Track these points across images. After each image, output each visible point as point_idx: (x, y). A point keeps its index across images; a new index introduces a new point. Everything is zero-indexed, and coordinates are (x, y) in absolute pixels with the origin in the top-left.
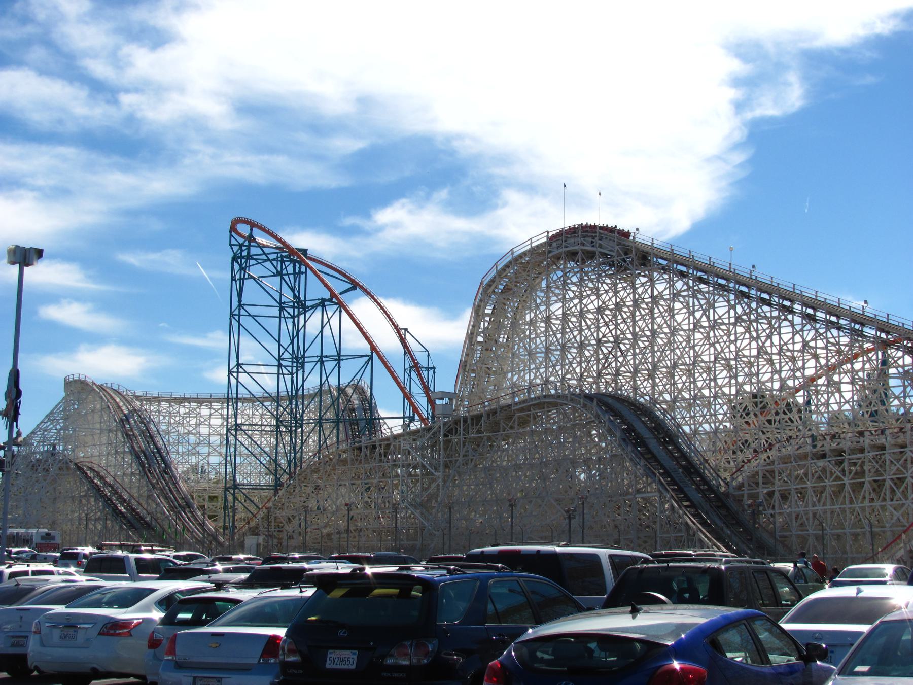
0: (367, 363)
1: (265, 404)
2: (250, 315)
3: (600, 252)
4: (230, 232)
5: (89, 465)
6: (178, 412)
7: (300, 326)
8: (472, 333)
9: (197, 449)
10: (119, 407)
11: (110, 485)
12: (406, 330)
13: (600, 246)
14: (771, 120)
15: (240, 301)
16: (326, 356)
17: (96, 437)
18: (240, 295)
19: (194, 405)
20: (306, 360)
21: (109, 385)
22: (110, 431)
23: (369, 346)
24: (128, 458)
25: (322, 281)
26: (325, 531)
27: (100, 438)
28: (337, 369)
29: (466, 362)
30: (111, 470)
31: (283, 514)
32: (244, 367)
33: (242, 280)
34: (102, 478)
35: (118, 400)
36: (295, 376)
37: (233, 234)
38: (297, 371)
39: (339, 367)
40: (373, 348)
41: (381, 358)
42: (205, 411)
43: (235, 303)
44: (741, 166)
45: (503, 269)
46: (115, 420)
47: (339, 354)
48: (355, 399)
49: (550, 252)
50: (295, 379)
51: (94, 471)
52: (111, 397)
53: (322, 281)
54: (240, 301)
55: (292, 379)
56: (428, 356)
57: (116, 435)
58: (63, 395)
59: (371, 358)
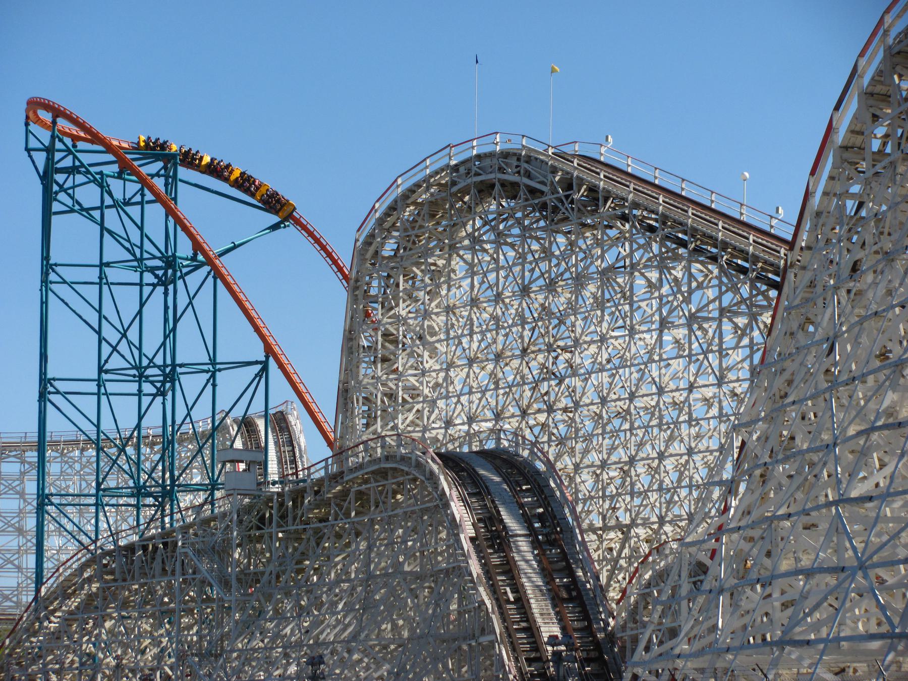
0: (259, 375)
2: (65, 282)
3: (527, 186)
13: (529, 175)
16: (181, 366)
20: (179, 370)
23: (261, 345)
28: (209, 387)
37: (33, 127)
39: (214, 386)
40: (269, 350)
41: (281, 366)
47: (213, 362)
49: (454, 183)
59: (265, 368)
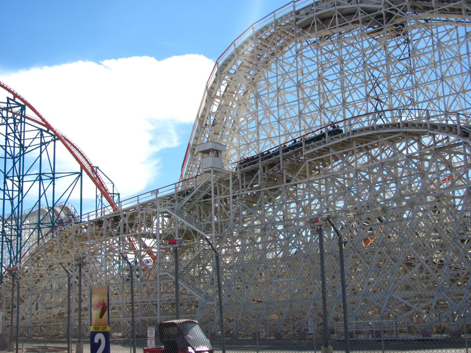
0: (79, 177)
7: (18, 163)
8: (203, 116)
12: (97, 168)
14: (167, 149)
23: (79, 166)
25: (40, 117)
28: (52, 185)
29: (195, 145)
36: (23, 130)
39: (54, 184)
44: (157, 165)
45: (225, 65)
48: (63, 215)
53: (40, 117)
56: (113, 185)
59: (81, 174)
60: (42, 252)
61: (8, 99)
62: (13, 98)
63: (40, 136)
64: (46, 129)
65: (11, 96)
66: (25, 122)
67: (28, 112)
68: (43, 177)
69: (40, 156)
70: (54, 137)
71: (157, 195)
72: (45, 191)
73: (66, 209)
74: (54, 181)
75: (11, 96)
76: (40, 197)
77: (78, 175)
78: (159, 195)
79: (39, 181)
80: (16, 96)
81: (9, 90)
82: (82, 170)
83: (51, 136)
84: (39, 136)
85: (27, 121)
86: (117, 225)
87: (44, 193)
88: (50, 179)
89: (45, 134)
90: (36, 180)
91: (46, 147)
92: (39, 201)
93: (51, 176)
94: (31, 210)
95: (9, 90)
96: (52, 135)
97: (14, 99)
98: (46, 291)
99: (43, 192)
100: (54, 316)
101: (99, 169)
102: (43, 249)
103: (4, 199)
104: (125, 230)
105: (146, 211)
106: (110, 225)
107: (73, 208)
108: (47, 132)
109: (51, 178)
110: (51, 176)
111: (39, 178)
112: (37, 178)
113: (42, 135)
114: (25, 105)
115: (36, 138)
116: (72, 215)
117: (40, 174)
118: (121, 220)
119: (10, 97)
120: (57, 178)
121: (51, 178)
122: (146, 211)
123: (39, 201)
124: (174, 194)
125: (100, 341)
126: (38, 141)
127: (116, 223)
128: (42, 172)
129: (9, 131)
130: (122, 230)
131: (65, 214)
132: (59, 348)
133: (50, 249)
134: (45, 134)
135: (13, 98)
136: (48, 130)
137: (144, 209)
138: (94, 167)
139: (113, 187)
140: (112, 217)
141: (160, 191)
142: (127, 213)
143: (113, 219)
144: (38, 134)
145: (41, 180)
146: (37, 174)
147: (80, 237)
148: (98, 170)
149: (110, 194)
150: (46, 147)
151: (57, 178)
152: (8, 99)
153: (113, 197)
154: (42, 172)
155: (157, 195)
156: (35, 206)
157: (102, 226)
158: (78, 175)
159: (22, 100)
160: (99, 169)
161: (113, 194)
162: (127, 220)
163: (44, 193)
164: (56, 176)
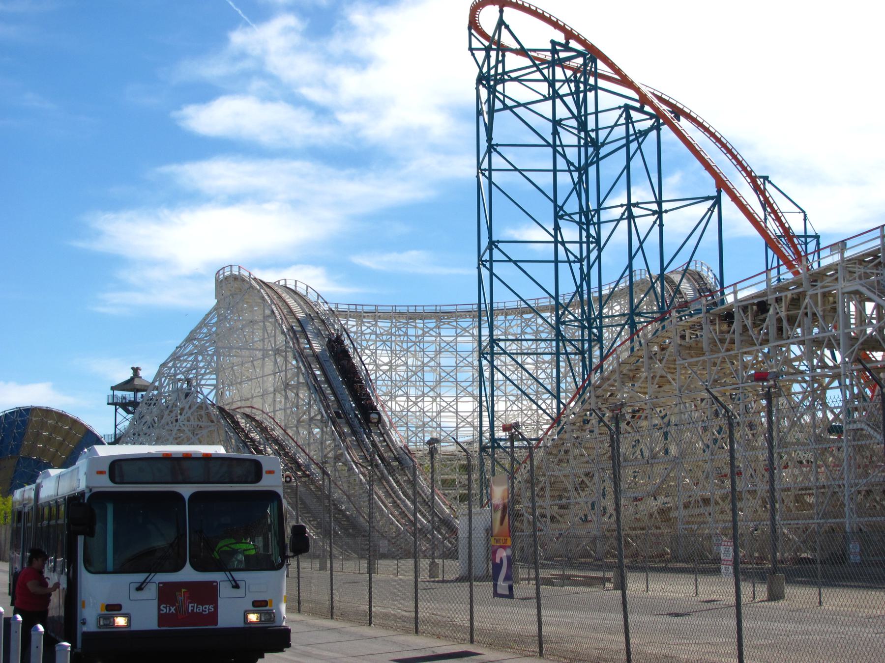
0: (713, 206)
1: (543, 315)
4: (470, 29)
5: (248, 411)
6: (406, 334)
9: (437, 390)
10: (291, 312)
11: (276, 441)
12: (766, 178)
15: (489, 139)
17: (257, 363)
18: (489, 129)
19: (431, 323)
21: (282, 283)
22: (277, 352)
23: (712, 181)
24: (304, 394)
26: (653, 505)
27: (263, 366)
28: (656, 228)
30: (280, 417)
31: (568, 471)
32: (500, 245)
33: (492, 111)
34: (263, 430)
35: (291, 302)
37: (473, 31)
38: (590, 347)
39: (661, 226)
42: (448, 333)
43: (484, 145)
46: (283, 332)
50: (585, 268)
51: (253, 419)
52: (280, 297)
54: (489, 139)
55: (581, 269)
56: (805, 216)
57: (286, 358)
58: (213, 302)
59: (717, 201)
60: (615, 381)
61: (553, 43)
62: (563, 41)
63: (624, 122)
64: (638, 105)
65: (560, 37)
66: (595, 88)
67: (601, 67)
68: (636, 211)
69: (628, 167)
70: (657, 121)
71: (842, 254)
72: (641, 243)
73: (697, 277)
74: (660, 218)
75: (560, 37)
76: (631, 258)
77: (710, 203)
78: (848, 254)
79: (626, 221)
80: (570, 35)
81: (556, 25)
82: (719, 192)
83: (651, 119)
84: (622, 121)
85: (601, 83)
86: (764, 320)
87: (641, 247)
88: (653, 214)
89: (635, 115)
90: (621, 219)
91: (640, 144)
92: (630, 266)
93: (655, 207)
94: (613, 286)
95: (556, 25)
96: (651, 116)
97: (567, 43)
98: (626, 464)
99: (638, 244)
100: (651, 515)
101: (770, 182)
102: (616, 376)
103: (556, 262)
104: (780, 330)
105: (823, 287)
106: (749, 323)
107: (711, 275)
108: (641, 110)
109: (654, 213)
110: (655, 207)
111: (626, 214)
112: (623, 214)
113: (629, 117)
114: (593, 53)
115: (616, 125)
116: (710, 290)
117: (629, 206)
118: (771, 311)
119: (557, 40)
120: (666, 211)
121: (654, 213)
122: (823, 287)
123: (630, 266)
124: (879, 249)
125: (501, 560)
126: (620, 131)
127: (762, 317)
128: (633, 201)
129: (562, 112)
130: (773, 331)
131: (694, 290)
132: (592, 578)
133: (631, 374)
134: (635, 115)
135: (563, 41)
136: (642, 107)
137: (819, 284)
138: (756, 177)
139: (805, 220)
140: (754, 304)
141: (849, 244)
142: (783, 294)
143: (755, 307)
144: (621, 116)
145: (631, 217)
146: (622, 206)
147: (690, 348)
148: (768, 186)
149: (798, 237)
150: (640, 144)
151: (666, 211)
152: (553, 43)
153: (806, 244)
154: (633, 201)
155: (842, 254)
156: (621, 278)
157: (732, 323)
158: (711, 202)
159: (583, 42)
160: (770, 182)
161: (806, 236)
162: (783, 309)
163: (641, 247)
164: (665, 206)
